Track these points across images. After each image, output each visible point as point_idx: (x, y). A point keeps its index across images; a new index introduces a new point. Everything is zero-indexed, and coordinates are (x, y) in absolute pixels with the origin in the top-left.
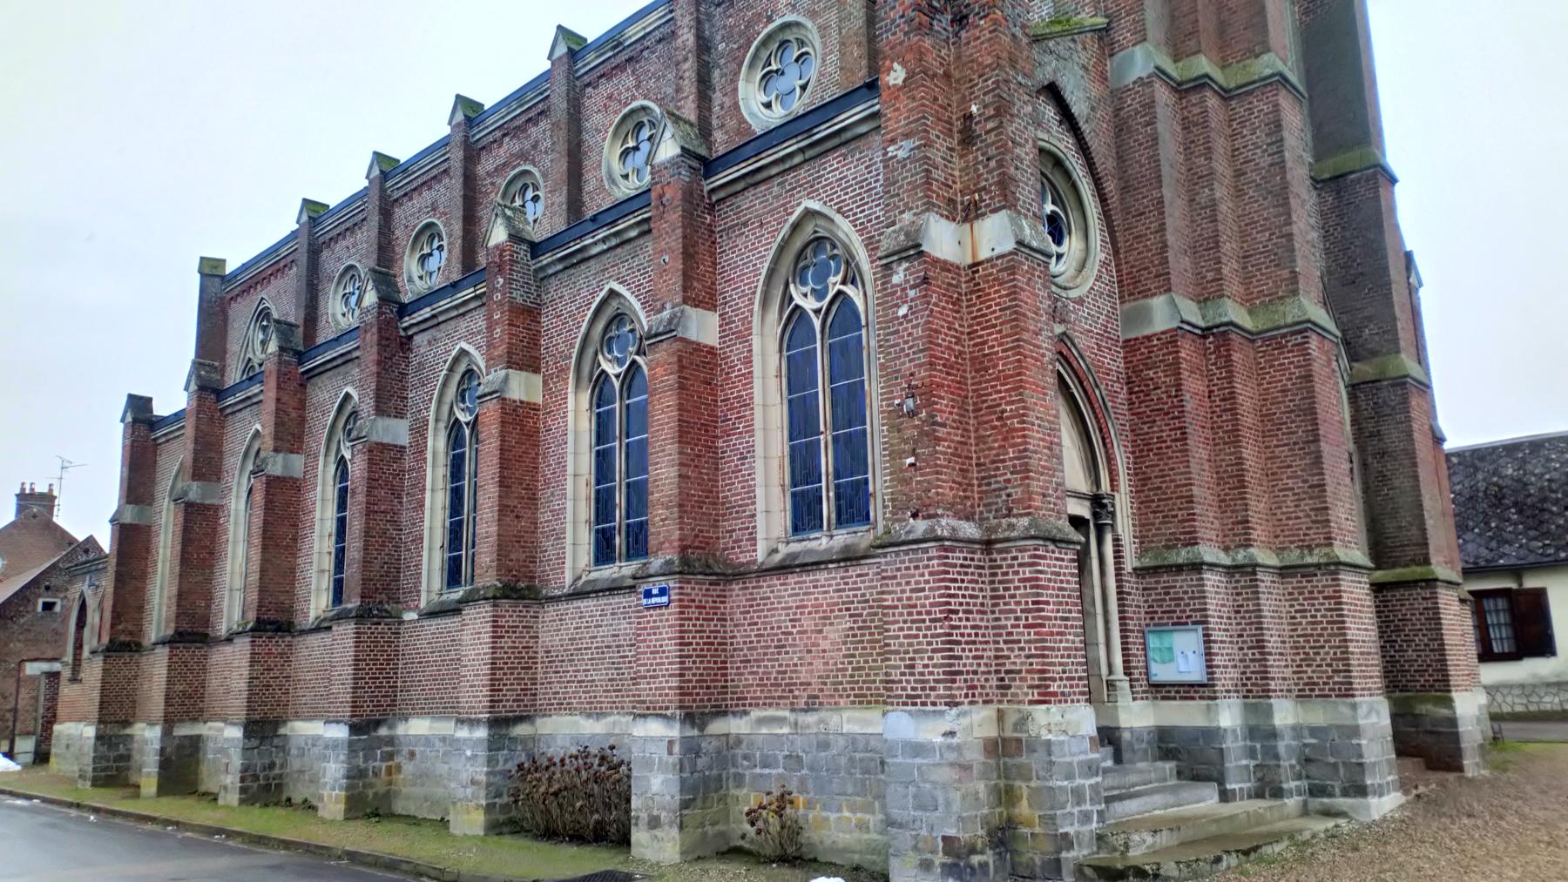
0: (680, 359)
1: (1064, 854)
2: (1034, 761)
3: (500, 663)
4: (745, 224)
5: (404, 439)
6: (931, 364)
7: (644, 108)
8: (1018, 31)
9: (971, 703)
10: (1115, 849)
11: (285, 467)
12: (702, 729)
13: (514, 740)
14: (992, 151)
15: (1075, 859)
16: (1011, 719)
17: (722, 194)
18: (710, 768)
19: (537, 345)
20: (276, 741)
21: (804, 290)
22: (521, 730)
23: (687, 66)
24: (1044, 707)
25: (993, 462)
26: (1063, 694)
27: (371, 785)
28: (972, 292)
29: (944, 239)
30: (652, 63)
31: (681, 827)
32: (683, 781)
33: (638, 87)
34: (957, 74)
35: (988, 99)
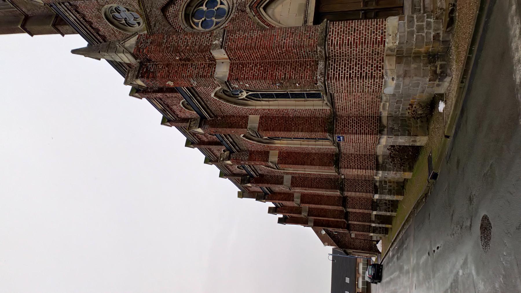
0: (264, 130)
1: (441, 39)
2: (405, 47)
3: (359, 167)
4: (220, 109)
5: (290, 177)
6: (264, 79)
7: (183, 103)
8: (149, 41)
9: (383, 69)
10: (442, 13)
11: (297, 198)
12: (384, 127)
13: (383, 162)
14: (191, 54)
15: (443, 33)
16: (389, 52)
17: (211, 114)
18: (398, 124)
19: (261, 152)
20: (378, 202)
21: (240, 95)
22: (380, 160)
23: (168, 95)
24: (386, 44)
25: (298, 55)
26: (382, 34)
27: (394, 188)
28: (239, 59)
29: (222, 71)
30: (169, 101)
31: (417, 136)
32: (402, 135)
33: (176, 105)
34: (167, 62)
35: (174, 55)
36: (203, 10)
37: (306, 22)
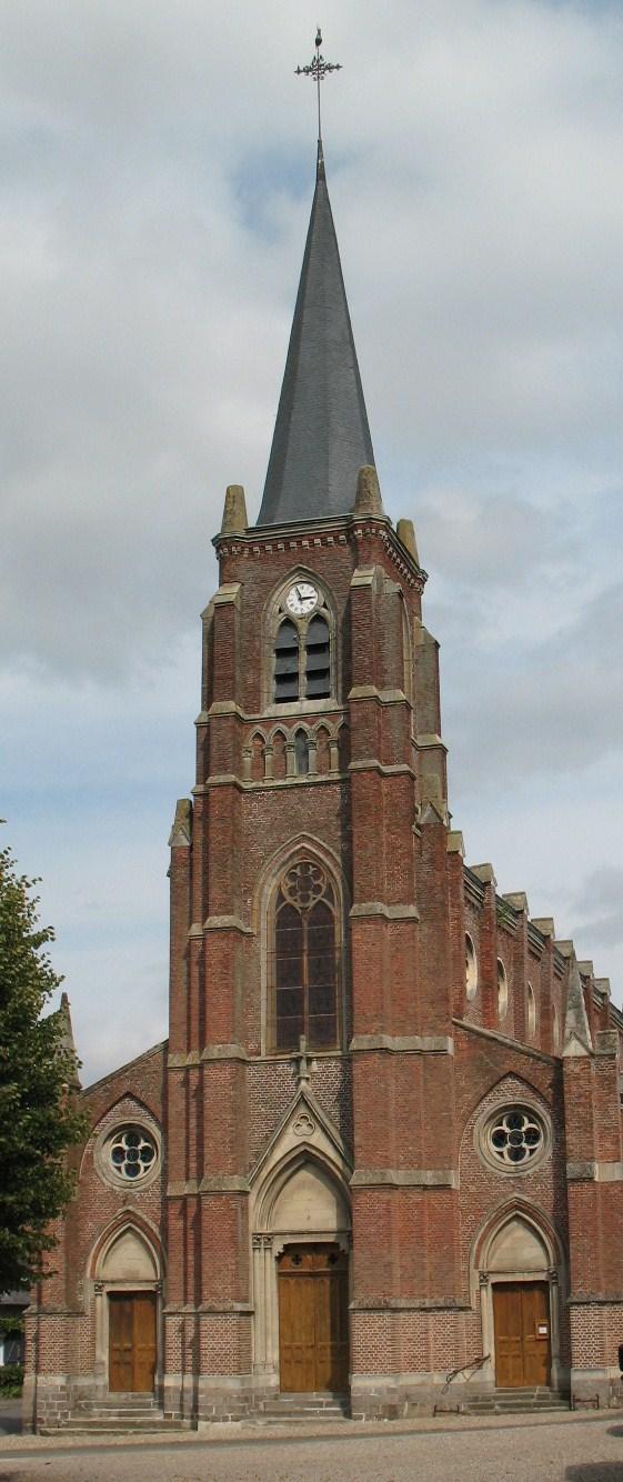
36: (521, 1124)
37: (113, 1282)
